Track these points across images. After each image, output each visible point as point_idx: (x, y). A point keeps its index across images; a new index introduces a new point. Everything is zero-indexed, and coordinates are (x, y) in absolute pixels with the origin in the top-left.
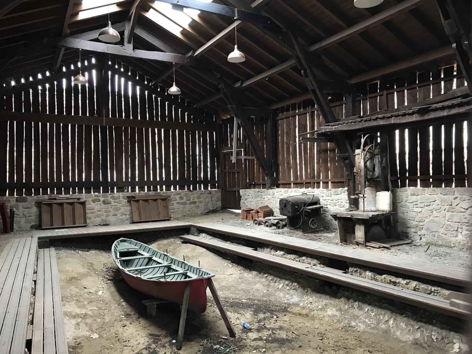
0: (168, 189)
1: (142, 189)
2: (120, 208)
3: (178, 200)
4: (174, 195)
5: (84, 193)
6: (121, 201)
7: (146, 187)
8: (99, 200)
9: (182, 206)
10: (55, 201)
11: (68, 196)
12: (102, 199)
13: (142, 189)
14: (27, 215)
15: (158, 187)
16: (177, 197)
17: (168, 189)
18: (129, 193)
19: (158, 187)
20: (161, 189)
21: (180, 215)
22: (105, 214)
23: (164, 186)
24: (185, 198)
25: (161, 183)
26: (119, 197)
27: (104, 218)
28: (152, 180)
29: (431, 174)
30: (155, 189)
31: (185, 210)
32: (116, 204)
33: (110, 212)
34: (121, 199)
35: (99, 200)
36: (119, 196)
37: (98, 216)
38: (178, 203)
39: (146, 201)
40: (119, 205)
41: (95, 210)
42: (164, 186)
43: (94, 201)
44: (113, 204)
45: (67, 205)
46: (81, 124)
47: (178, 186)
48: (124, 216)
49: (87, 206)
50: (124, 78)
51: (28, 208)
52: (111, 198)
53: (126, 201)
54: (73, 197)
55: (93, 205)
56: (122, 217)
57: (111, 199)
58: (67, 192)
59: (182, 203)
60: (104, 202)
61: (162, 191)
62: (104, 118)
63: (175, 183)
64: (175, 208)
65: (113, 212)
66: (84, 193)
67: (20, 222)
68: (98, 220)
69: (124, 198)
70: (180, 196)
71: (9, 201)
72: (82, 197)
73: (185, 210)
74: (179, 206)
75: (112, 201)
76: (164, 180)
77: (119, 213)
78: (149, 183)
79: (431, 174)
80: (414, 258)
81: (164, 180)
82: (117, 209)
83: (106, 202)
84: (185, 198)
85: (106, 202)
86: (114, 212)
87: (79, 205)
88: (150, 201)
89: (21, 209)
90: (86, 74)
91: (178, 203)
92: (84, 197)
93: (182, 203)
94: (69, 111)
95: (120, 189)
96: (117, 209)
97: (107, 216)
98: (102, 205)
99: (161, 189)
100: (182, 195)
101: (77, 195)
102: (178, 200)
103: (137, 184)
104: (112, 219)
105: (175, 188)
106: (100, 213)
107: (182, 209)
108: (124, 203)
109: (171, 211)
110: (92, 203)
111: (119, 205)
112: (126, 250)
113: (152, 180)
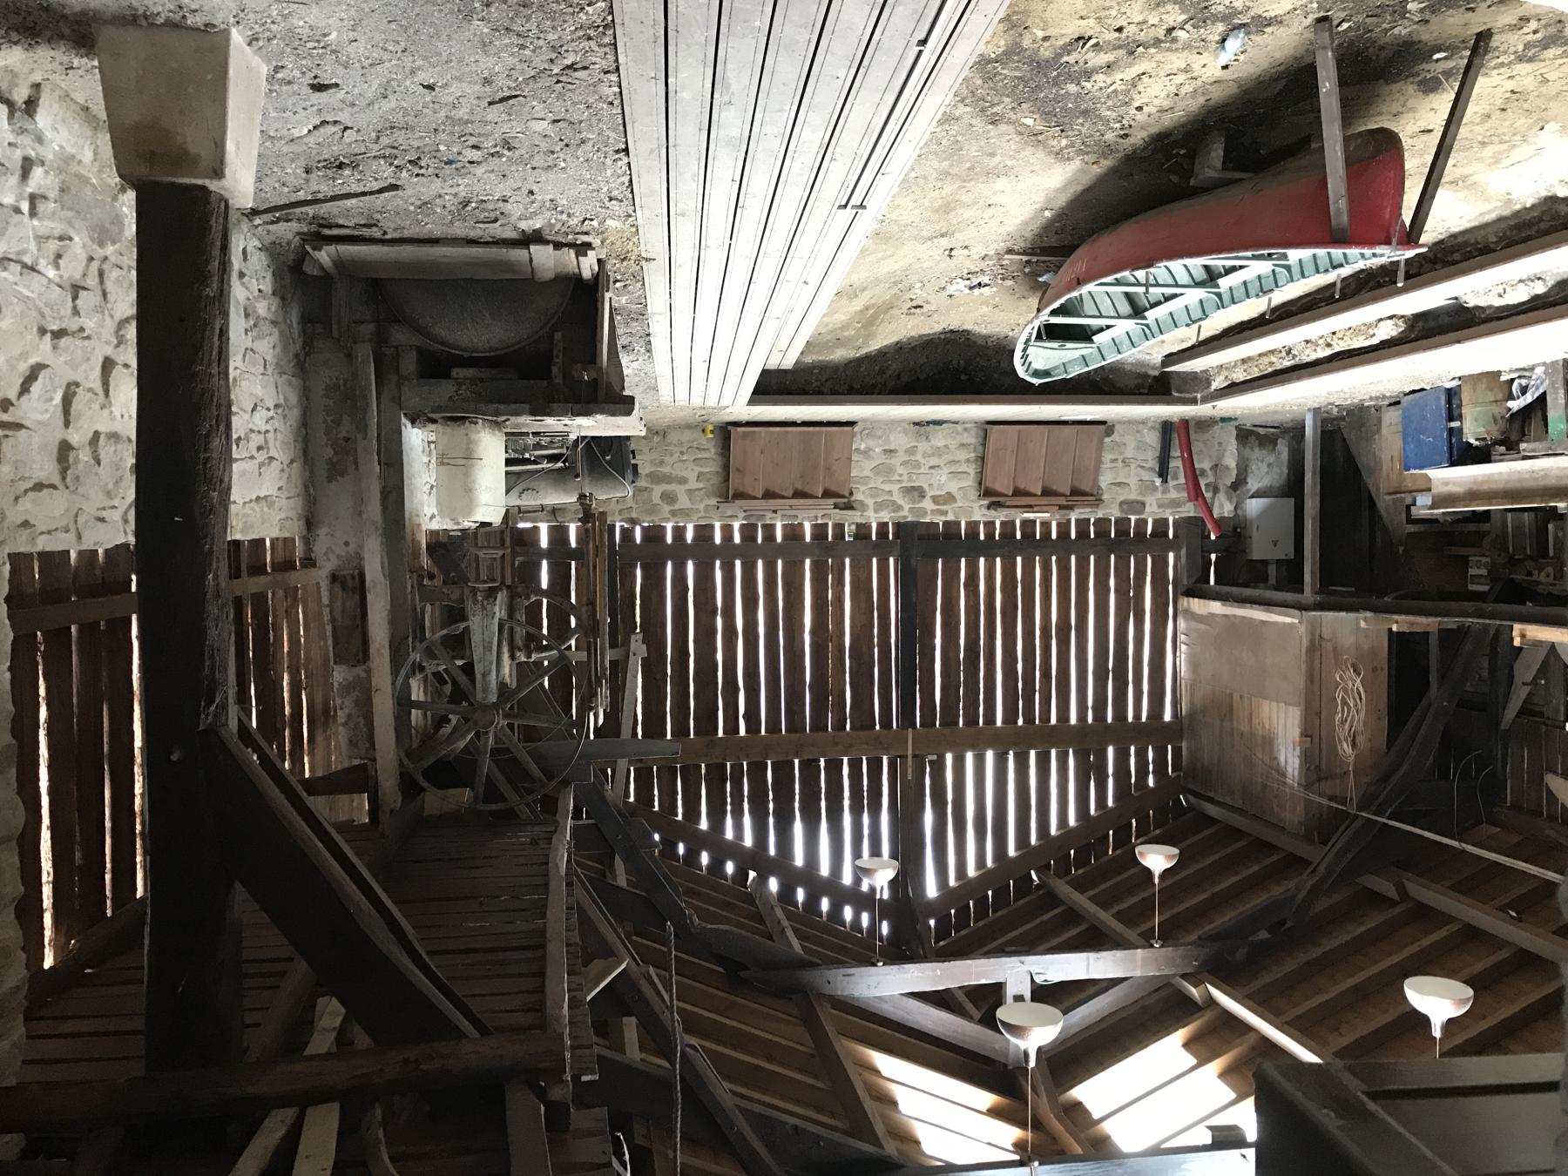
0: (704, 532)
1: (793, 533)
2: (877, 474)
3: (680, 490)
4: (697, 510)
5: (1150, 522)
6: (872, 496)
7: (779, 539)
8: (935, 499)
9: (666, 470)
10: (1062, 501)
11: (1026, 515)
12: (927, 504)
13: (793, 533)
14: (1120, 464)
15: (737, 539)
16: (683, 502)
17: (704, 532)
18: (850, 521)
19: (737, 539)
20: (727, 531)
21: (674, 437)
22: (919, 457)
23: (718, 540)
24: (656, 498)
25: (728, 552)
26: (878, 507)
27: (923, 447)
28: (760, 563)
29: (545, 564)
30: (749, 532)
31: (655, 456)
32: (887, 487)
33: (904, 463)
34: (870, 502)
35: (935, 499)
36: (876, 511)
37: (938, 452)
38: (683, 481)
39: (799, 494)
40: (877, 482)
41: (946, 470)
42: (718, 540)
43: (950, 498)
44: (895, 488)
45: (1032, 490)
46: (792, 736)
47: (982, 537)
48: (863, 447)
49: (969, 482)
50: (844, 887)
51: (1119, 484)
52: (900, 508)
53: (858, 496)
54: (1012, 511)
55: (953, 487)
56: (871, 443)
57: (900, 502)
58: (1008, 526)
59: (668, 479)
60: (919, 492)
61: (729, 524)
62: (910, 752)
63: (680, 551)
64: (692, 466)
65: (896, 461)
66: (1150, 522)
67: (1138, 448)
68: (940, 438)
69: (864, 507)
70: (677, 507)
71: (1160, 506)
72: (984, 511)
73: (655, 456)
74: (678, 471)
75: (898, 498)
76: (718, 563)
77: (878, 458)
78: (770, 551)
79: (545, 564)
80: (87, 156)
81: (718, 563)
82: (884, 471)
83: (916, 494)
84: (656, 498)
85: (916, 494)
86: (893, 461)
87: (998, 487)
88: (790, 493)
89: (1133, 481)
90: (865, 887)
91: (683, 481)
92: (976, 509)
93: (668, 479)
94: (783, 770)
95: (862, 532)
96: (884, 471)
97: (912, 451)
98: (926, 487)
99: (727, 531)
100: (667, 508)
101: (999, 517)
102: (680, 490)
103: (781, 551)
104: (900, 441)
105: (679, 532)
106: (934, 461)
107: (667, 459)
108: (862, 488)
109: (707, 455)
110: (954, 492)
111: (877, 482)
112: (1069, 345)
113: (760, 563)
